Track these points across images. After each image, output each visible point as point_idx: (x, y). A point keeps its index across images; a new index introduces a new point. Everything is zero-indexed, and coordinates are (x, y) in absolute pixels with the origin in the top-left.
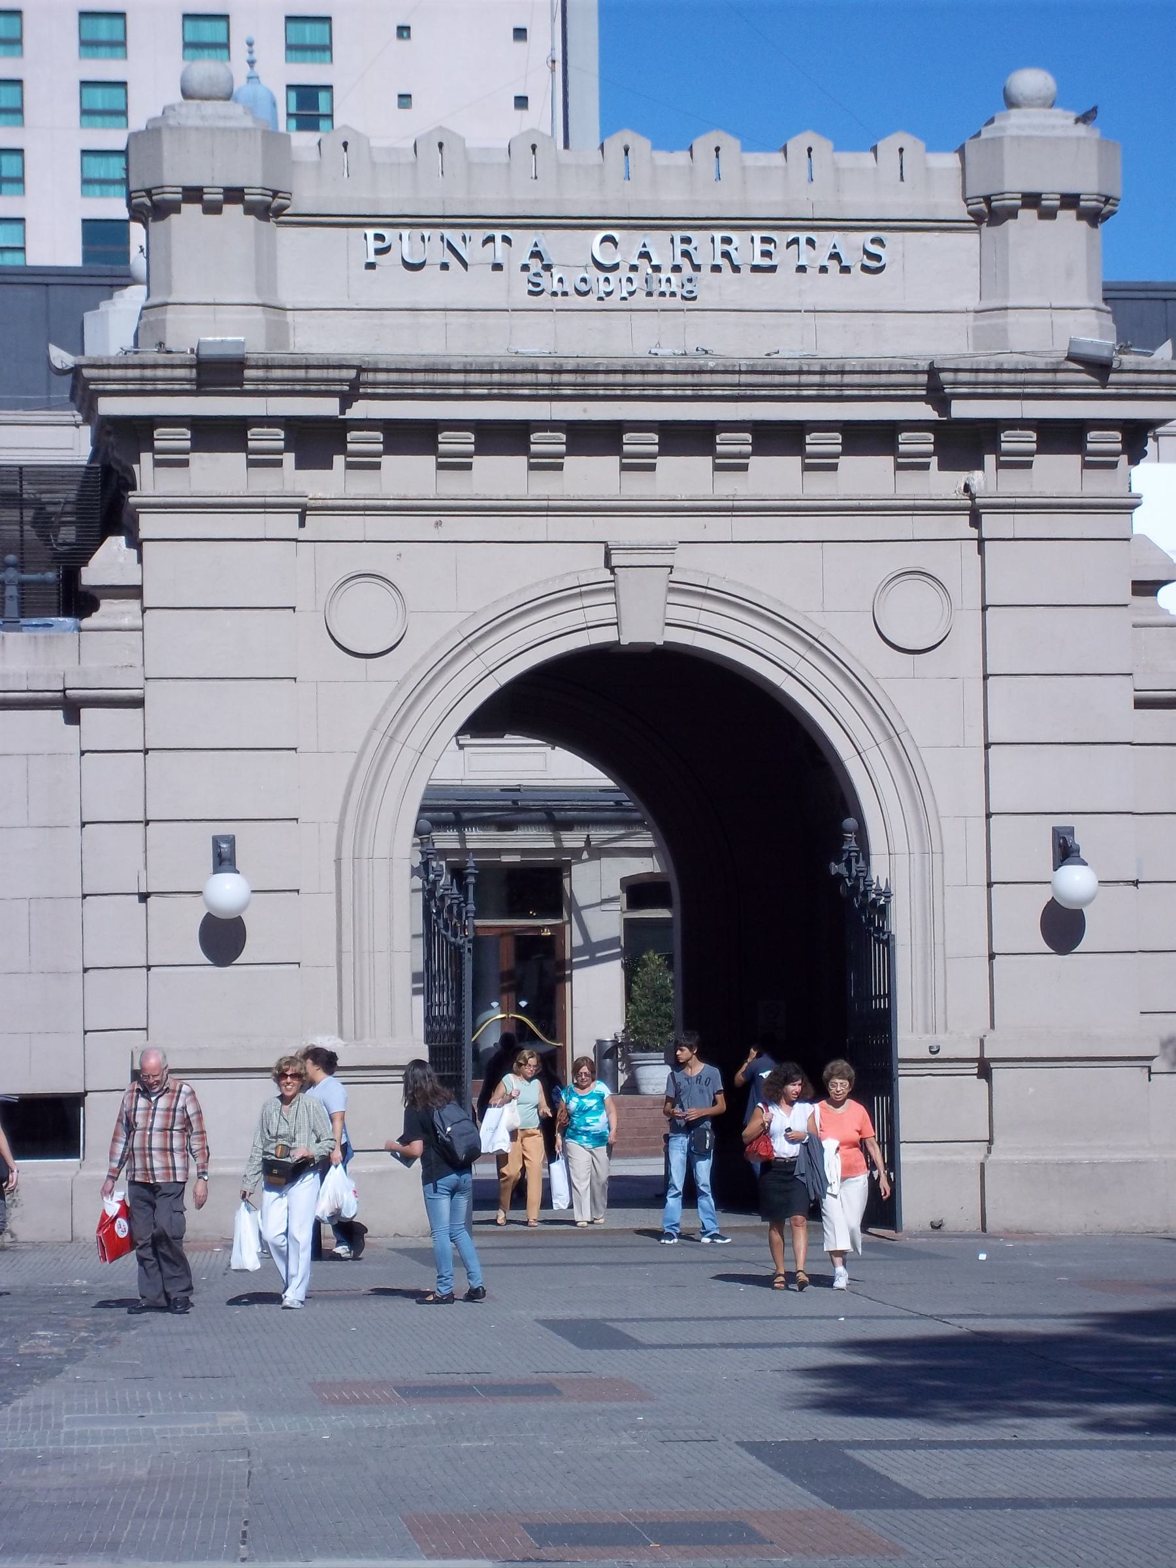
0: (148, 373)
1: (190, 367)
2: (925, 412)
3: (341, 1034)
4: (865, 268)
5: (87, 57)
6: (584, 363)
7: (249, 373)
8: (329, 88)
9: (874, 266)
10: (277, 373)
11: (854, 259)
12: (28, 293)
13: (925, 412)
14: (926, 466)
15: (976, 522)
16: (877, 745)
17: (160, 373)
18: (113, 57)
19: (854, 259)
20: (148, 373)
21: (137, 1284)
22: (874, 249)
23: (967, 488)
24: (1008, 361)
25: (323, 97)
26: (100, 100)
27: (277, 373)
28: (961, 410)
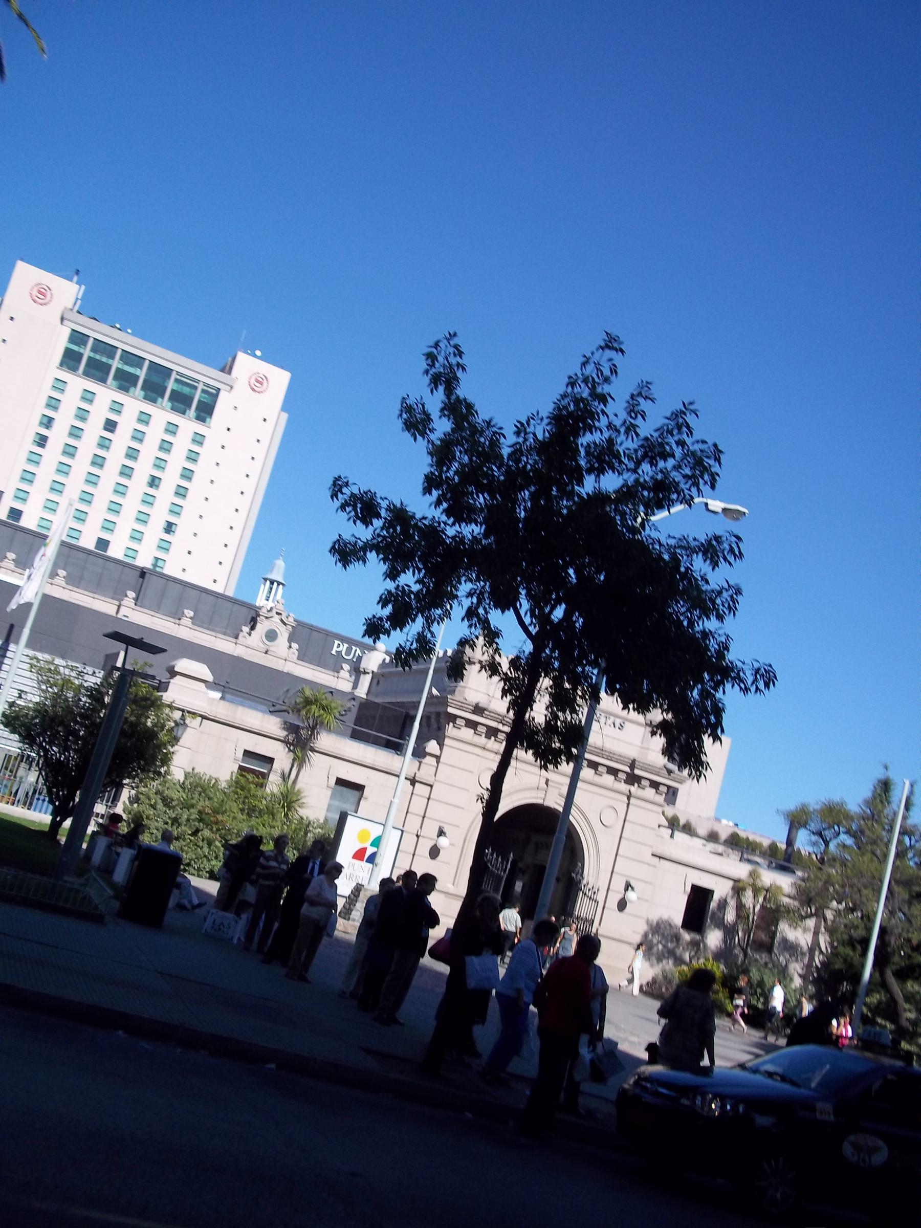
0: (463, 705)
1: (472, 706)
2: (628, 770)
3: (453, 884)
4: (619, 728)
5: (28, 463)
6: (654, 765)
7: (486, 712)
8: (176, 525)
9: (621, 727)
10: (492, 714)
11: (617, 725)
12: (212, 597)
13: (628, 770)
14: (621, 781)
15: (629, 798)
16: (429, 799)
17: (466, 706)
18: (121, 497)
19: (617, 725)
20: (463, 705)
21: (359, 924)
22: (622, 724)
23: (630, 791)
24: (648, 762)
25: (174, 526)
26: (114, 507)
27: (492, 714)
28: (637, 772)
